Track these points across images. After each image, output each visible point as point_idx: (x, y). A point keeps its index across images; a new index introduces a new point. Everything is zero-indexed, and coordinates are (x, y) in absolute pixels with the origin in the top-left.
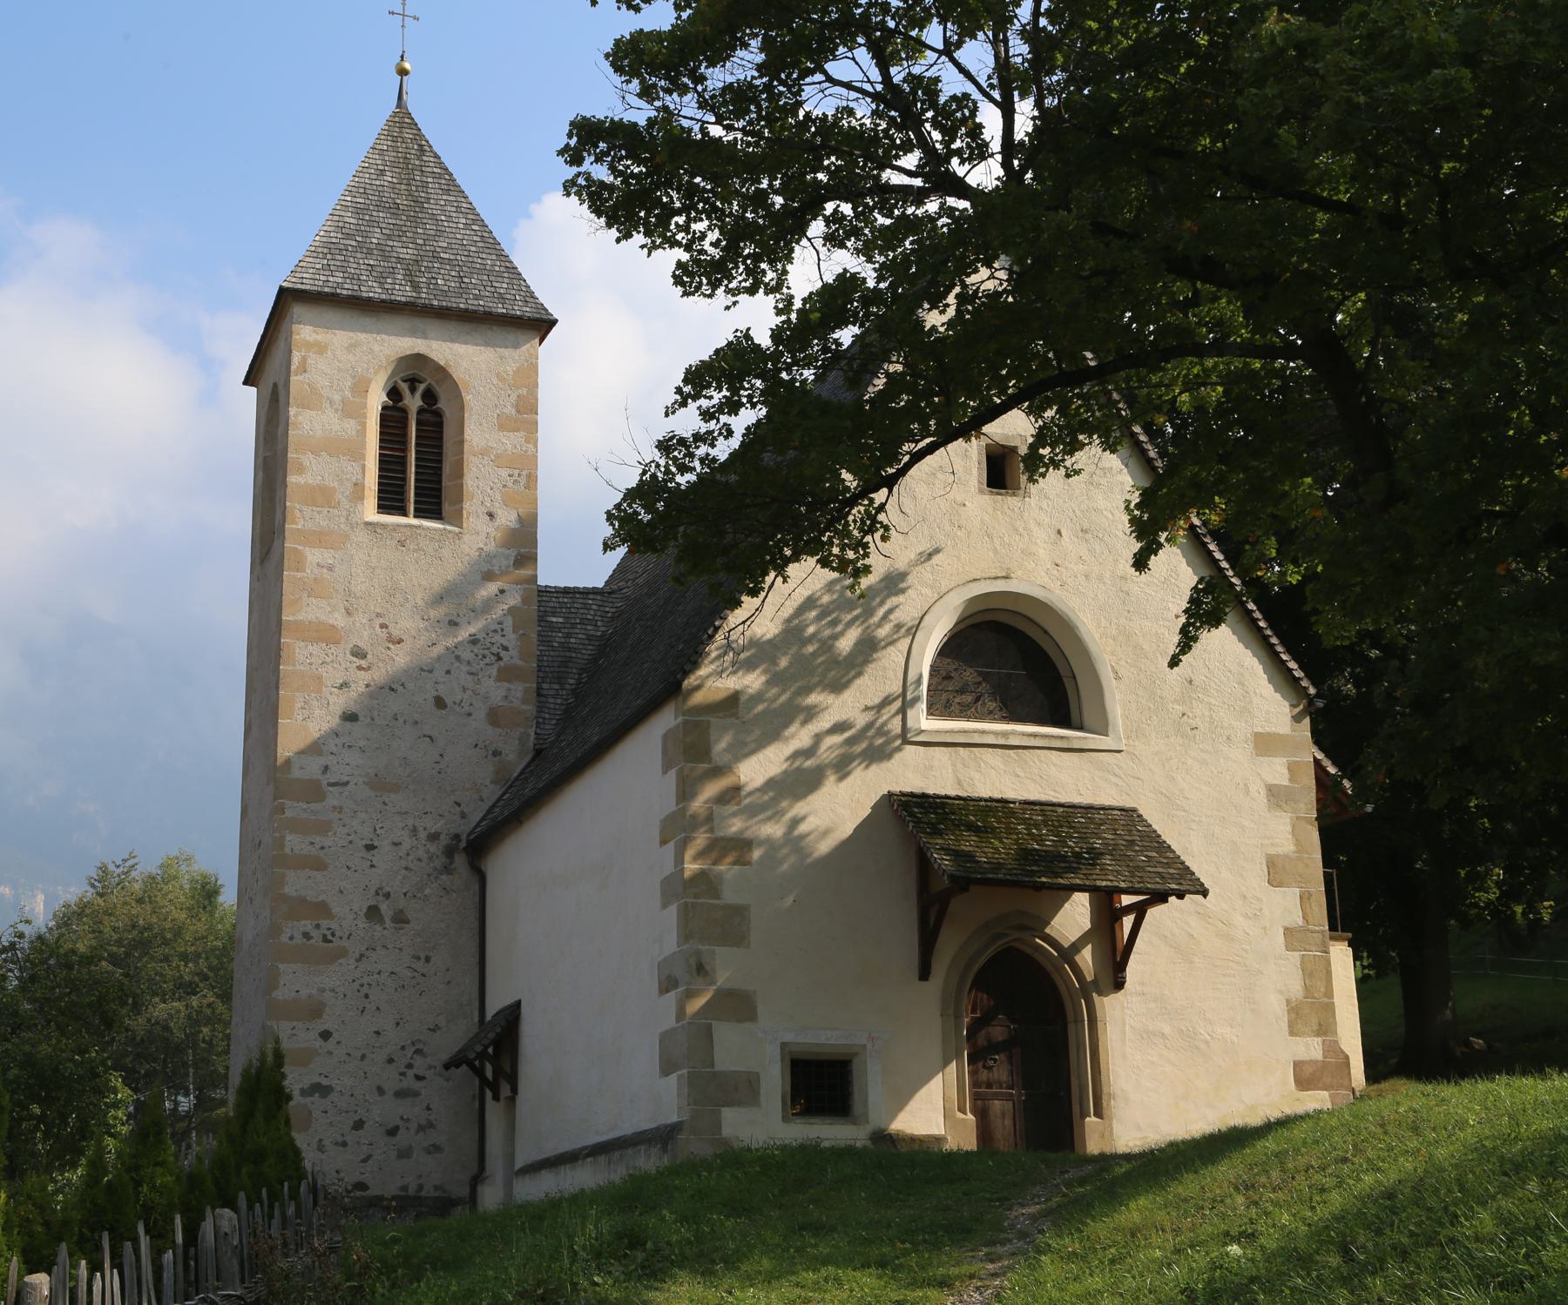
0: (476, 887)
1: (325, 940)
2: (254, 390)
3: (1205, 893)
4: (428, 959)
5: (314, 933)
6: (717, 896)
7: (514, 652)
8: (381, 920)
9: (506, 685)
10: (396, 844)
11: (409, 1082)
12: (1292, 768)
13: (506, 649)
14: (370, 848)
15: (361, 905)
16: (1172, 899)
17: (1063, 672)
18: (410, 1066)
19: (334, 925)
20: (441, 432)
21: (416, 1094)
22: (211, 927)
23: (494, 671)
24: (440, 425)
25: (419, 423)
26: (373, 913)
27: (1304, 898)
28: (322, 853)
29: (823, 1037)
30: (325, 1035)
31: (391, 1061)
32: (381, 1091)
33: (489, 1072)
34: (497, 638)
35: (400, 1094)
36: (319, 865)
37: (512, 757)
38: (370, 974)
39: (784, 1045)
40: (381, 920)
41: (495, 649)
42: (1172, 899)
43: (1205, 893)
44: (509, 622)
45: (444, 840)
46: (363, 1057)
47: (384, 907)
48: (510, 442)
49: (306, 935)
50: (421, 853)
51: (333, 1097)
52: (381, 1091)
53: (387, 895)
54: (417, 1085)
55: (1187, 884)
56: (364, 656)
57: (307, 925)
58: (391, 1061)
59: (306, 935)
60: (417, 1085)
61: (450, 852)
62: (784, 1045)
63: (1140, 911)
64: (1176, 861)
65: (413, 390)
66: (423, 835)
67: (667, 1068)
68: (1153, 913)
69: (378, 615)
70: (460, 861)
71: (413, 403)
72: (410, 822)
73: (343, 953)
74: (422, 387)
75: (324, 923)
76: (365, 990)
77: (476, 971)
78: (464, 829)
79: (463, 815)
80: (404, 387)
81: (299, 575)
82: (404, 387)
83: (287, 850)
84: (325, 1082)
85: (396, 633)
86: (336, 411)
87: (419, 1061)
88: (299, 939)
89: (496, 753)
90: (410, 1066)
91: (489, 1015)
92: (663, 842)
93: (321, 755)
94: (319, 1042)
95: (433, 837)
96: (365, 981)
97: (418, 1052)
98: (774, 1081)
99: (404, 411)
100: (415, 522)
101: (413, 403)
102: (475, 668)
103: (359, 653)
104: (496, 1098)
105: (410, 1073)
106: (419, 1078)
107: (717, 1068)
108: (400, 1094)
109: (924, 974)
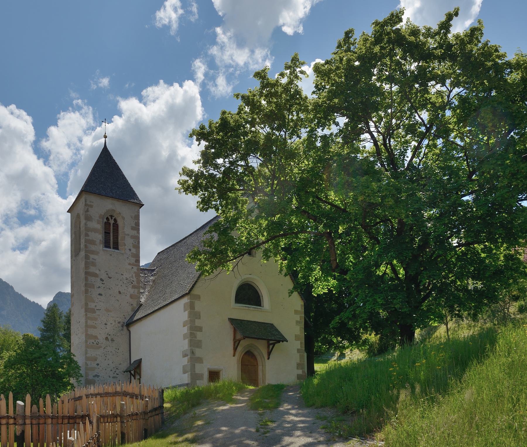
0: (128, 334)
1: (97, 344)
2: (70, 214)
3: (287, 341)
4: (118, 349)
5: (95, 342)
6: (196, 338)
7: (135, 282)
8: (108, 340)
9: (134, 289)
10: (111, 324)
11: (115, 375)
12: (300, 317)
13: (133, 281)
14: (106, 324)
15: (104, 337)
16: (281, 342)
17: (260, 295)
18: (115, 372)
19: (99, 341)
20: (118, 229)
21: (117, 378)
22: (490, 307)
23: (131, 286)
24: (118, 227)
25: (113, 226)
26: (107, 339)
27: (301, 343)
28: (96, 325)
29: (215, 367)
30: (98, 364)
31: (111, 370)
32: (109, 377)
33: (132, 372)
34: (132, 279)
35: (113, 377)
36: (95, 327)
37: (135, 306)
38: (106, 352)
39: (208, 368)
40: (108, 340)
41: (131, 281)
42: (281, 342)
43: (287, 341)
44: (134, 275)
45: (121, 323)
46: (106, 369)
47: (109, 337)
48: (134, 233)
49: (93, 343)
50: (117, 326)
51: (100, 377)
52: (109, 377)
53: (110, 335)
54: (117, 376)
55: (285, 340)
56: (103, 281)
57: (93, 341)
58: (111, 370)
59: (93, 343)
60: (117, 376)
61: (122, 326)
62: (208, 368)
63: (274, 344)
64: (281, 335)
65: (112, 218)
66: (117, 322)
67: (185, 372)
68: (276, 345)
69: (106, 271)
70: (125, 328)
71: (112, 222)
72: (114, 319)
73: (101, 347)
74: (113, 218)
75: (97, 340)
76: (106, 355)
77: (129, 352)
78: (126, 321)
79: (125, 318)
80: (110, 218)
81: (88, 261)
82: (110, 218)
83: (88, 324)
84: (98, 374)
85: (110, 276)
86: (457, 100)
87: (117, 371)
88: (91, 343)
89: (132, 305)
90: (115, 372)
91: (132, 362)
92: (184, 326)
93: (94, 302)
94: (96, 366)
95: (119, 323)
96: (106, 353)
97: (117, 369)
98: (206, 375)
99: (110, 224)
100: (113, 250)
101: (112, 222)
102: (127, 285)
103: (102, 280)
104: (135, 379)
105: (115, 373)
106: (117, 374)
107: (196, 372)
108: (113, 377)
109: (234, 356)
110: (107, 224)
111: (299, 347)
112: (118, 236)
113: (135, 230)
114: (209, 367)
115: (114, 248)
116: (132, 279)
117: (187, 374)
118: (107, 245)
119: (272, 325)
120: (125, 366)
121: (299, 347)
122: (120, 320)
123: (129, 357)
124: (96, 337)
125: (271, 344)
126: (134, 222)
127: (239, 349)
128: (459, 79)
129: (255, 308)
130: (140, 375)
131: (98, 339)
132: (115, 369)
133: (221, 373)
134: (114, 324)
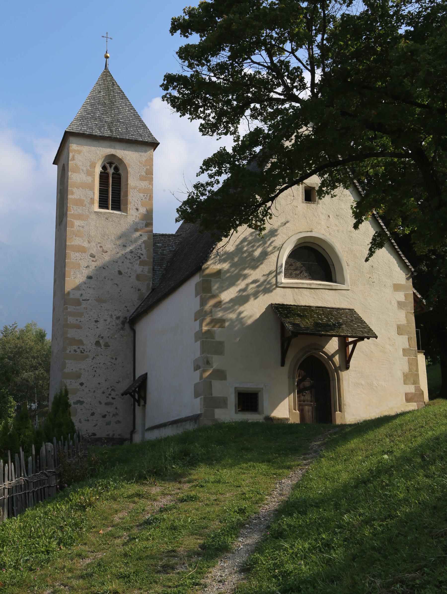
0: (132, 335)
1: (81, 352)
2: (57, 166)
3: (376, 337)
4: (116, 359)
5: (78, 350)
6: (214, 339)
9: (142, 267)
10: (105, 320)
11: (110, 400)
12: (406, 296)
13: (142, 255)
14: (96, 321)
16: (366, 339)
17: (330, 263)
18: (110, 395)
19: (84, 347)
20: (120, 181)
24: (120, 179)
26: (98, 343)
30: (82, 384)
31: (104, 393)
32: (100, 403)
35: (107, 404)
36: (79, 327)
37: (144, 291)
38: (97, 364)
41: (138, 255)
42: (366, 339)
43: (376, 337)
45: (121, 319)
46: (94, 392)
47: (101, 342)
48: (143, 184)
52: (100, 403)
53: (102, 337)
55: (370, 334)
56: (94, 257)
57: (75, 347)
59: (75, 351)
61: (123, 323)
63: (355, 343)
65: (111, 167)
66: (114, 317)
70: (127, 326)
72: (110, 313)
73: (87, 357)
75: (81, 347)
76: (95, 369)
77: (132, 363)
78: (128, 315)
79: (128, 311)
81: (72, 229)
82: (108, 166)
83: (69, 322)
84: (81, 400)
85: (105, 249)
88: (72, 352)
90: (110, 395)
91: (137, 377)
94: (79, 387)
95: (118, 318)
96: (95, 366)
97: (113, 390)
98: (232, 400)
99: (108, 174)
100: (112, 211)
101: (111, 171)
104: (139, 405)
105: (110, 397)
106: (113, 398)
108: (107, 404)
109: (283, 364)
110: (104, 177)
111: (407, 346)
112: (120, 191)
113: (146, 180)
114: (237, 385)
115: (113, 209)
116: (139, 251)
117: (199, 399)
118: (103, 204)
119: (352, 311)
120: (125, 385)
121: (407, 346)
122: (120, 314)
123: (132, 370)
124: (80, 342)
125: (351, 343)
126: (145, 169)
127: (291, 355)
128: (269, 11)
129: (320, 285)
130: (145, 399)
131: (83, 344)
132: (110, 390)
133: (259, 395)
134: (109, 320)
